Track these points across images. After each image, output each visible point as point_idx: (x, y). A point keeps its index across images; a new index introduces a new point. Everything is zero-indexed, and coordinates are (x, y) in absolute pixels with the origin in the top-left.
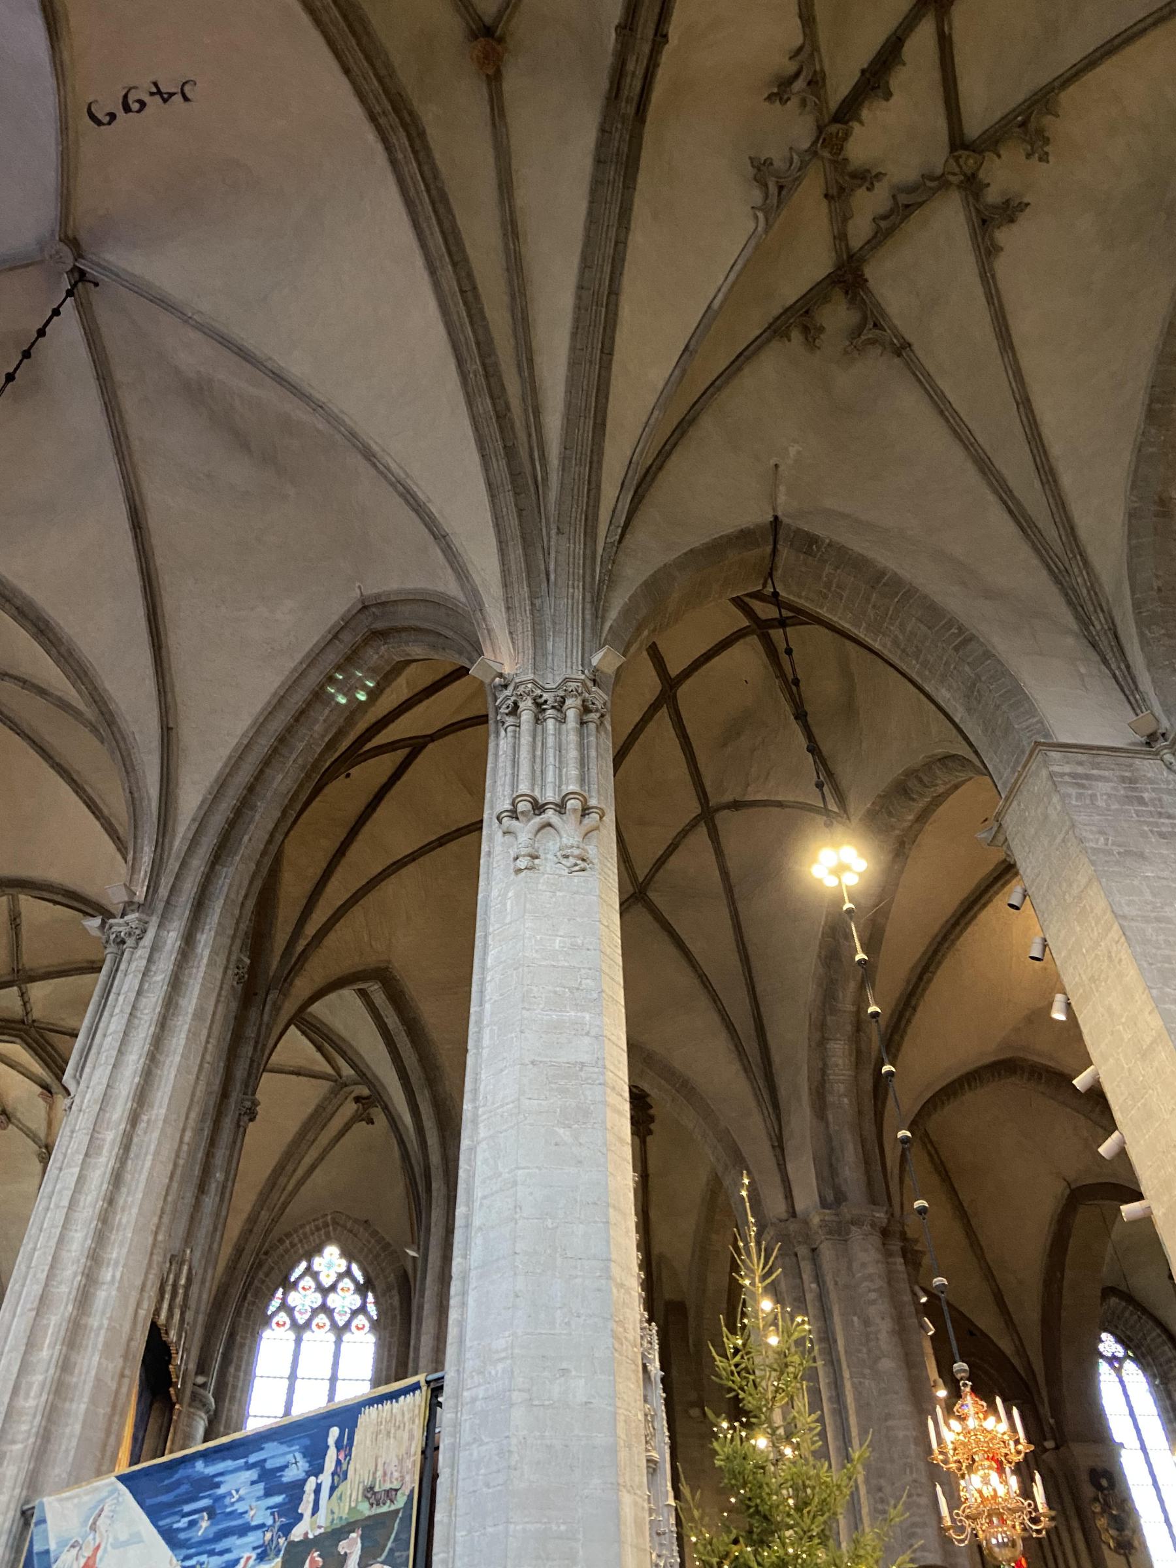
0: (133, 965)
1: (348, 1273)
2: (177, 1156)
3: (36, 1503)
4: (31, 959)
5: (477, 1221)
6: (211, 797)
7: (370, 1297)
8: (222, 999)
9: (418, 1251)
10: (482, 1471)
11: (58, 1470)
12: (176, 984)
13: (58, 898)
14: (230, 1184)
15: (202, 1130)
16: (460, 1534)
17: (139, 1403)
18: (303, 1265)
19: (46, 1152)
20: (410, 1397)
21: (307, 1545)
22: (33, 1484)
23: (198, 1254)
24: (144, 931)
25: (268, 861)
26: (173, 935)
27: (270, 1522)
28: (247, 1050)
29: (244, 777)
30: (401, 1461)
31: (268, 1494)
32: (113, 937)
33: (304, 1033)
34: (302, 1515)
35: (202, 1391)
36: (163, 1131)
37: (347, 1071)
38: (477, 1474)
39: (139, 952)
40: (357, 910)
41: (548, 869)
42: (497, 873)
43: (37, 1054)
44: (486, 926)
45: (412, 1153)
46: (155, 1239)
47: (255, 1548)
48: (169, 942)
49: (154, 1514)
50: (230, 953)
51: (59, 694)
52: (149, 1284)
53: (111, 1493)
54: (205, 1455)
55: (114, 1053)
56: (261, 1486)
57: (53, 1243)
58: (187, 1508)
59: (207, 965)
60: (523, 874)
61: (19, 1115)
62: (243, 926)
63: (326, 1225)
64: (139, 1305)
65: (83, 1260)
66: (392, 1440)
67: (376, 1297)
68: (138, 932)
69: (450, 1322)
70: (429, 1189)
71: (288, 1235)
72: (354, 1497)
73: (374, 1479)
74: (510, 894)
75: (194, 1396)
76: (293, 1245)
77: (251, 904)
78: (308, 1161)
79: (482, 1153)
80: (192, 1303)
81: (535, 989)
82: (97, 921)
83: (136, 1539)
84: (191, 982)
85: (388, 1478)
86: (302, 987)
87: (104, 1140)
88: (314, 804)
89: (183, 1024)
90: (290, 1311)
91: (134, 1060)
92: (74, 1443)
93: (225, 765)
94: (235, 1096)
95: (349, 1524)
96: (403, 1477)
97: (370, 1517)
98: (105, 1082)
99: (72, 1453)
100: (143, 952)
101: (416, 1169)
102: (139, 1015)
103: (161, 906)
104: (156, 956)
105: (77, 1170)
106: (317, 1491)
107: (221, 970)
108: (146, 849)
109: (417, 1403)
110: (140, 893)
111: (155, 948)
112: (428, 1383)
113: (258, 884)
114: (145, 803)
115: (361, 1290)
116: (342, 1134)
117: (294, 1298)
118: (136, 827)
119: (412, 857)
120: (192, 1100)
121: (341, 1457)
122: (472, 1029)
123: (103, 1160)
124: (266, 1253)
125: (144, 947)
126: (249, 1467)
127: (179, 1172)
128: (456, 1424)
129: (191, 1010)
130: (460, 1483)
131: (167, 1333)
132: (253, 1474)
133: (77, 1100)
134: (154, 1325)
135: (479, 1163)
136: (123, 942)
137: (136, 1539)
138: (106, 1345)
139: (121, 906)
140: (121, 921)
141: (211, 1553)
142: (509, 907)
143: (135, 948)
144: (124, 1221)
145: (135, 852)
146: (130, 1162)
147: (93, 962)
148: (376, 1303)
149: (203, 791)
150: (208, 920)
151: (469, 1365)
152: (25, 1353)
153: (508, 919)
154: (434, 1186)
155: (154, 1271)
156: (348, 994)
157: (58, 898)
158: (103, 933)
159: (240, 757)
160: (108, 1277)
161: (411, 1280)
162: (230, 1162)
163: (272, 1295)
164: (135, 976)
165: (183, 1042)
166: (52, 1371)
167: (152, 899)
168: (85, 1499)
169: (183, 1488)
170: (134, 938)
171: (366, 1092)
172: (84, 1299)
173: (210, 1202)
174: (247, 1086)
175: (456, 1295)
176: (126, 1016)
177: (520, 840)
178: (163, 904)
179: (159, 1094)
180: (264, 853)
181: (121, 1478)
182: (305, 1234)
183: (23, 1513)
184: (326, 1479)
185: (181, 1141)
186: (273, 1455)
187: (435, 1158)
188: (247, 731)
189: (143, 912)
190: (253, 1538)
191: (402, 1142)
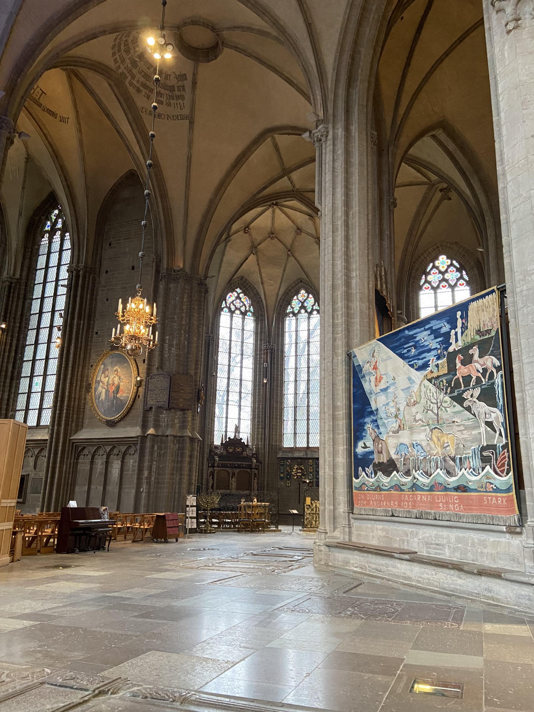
0: (328, 149)
1: (452, 265)
2: (368, 226)
3: (351, 351)
4: (289, 163)
5: (512, 219)
6: (338, 54)
7: (464, 273)
8: (369, 154)
9: (483, 248)
10: (530, 317)
11: (356, 340)
12: (348, 153)
13: (290, 131)
14: (392, 235)
15: (375, 215)
16: (523, 341)
17: (378, 318)
18: (431, 265)
19: (318, 240)
20: (490, 296)
21: (455, 353)
22: (349, 346)
23: (387, 263)
24: (328, 132)
25: (373, 80)
26: (340, 130)
27: (439, 347)
28: (385, 177)
29: (350, 38)
30: (491, 319)
31: (436, 338)
32: (316, 139)
33: (409, 165)
34: (451, 343)
35: (401, 316)
36: (359, 218)
37: (434, 178)
38: (528, 319)
39: (328, 143)
40: (423, 94)
41: (527, 25)
42: (496, 38)
43: (302, 202)
44: (494, 71)
45: (472, 207)
46: (368, 259)
47: (435, 356)
48: (339, 134)
49: (393, 349)
50: (367, 131)
51: (257, 27)
52: (370, 275)
53: (376, 345)
54: (408, 328)
55: (331, 189)
56: (433, 335)
57: (331, 267)
58: (405, 346)
59: (359, 140)
60: (512, 33)
61: (304, 228)
62: (369, 117)
63: (438, 247)
64: (368, 284)
65: (343, 270)
66: (485, 312)
67: (466, 272)
68: (325, 133)
69: (505, 264)
70: (484, 221)
71: (422, 254)
72: (472, 334)
73: (480, 327)
74: (506, 47)
75: (398, 318)
76: (425, 258)
77: (370, 104)
78: (423, 222)
79: (511, 187)
80: (389, 281)
81: (529, 97)
82: (307, 134)
83: (389, 358)
84: (354, 150)
85: (486, 326)
86: (404, 141)
87: (338, 225)
88: (388, 42)
89: (355, 170)
90: (429, 283)
91: (340, 164)
92: (358, 332)
93: (340, 35)
94: (385, 199)
95: (471, 344)
96: (492, 325)
97: (480, 340)
98: (331, 202)
99: (359, 335)
100: (330, 142)
101: (476, 213)
102: (336, 170)
103: (331, 118)
104: (336, 142)
105: (331, 238)
106: (456, 334)
107: (365, 141)
108: (317, 92)
109: (494, 297)
110: (321, 114)
111: (334, 139)
112: (498, 289)
113: (371, 92)
114: (310, 68)
115: (459, 270)
116: (437, 206)
117: (429, 278)
118: (310, 83)
119: (447, 54)
120: (368, 202)
121: (464, 321)
122: (495, 128)
123: (339, 232)
124: (414, 262)
125: (330, 140)
126: (426, 330)
127: (370, 231)
128: (514, 303)
129: (357, 162)
130: (520, 323)
131: (382, 293)
132: (428, 332)
133: (323, 212)
134: (376, 290)
135: (509, 193)
136: (321, 140)
137: (389, 358)
138: (361, 299)
139: (315, 123)
140: (317, 130)
141: (419, 359)
142: (506, 55)
143: (326, 141)
144: (354, 254)
145: (313, 96)
146: (350, 232)
147: (311, 157)
148: (467, 274)
149: (334, 53)
150: (353, 118)
151: (517, 278)
152: (333, 305)
153: (507, 63)
154: (487, 219)
155: (371, 270)
156: (427, 139)
157: (290, 131)
158: (311, 138)
159: (346, 27)
160: (354, 275)
161: (482, 262)
162: (390, 226)
163: (421, 279)
164: (330, 154)
165: (357, 178)
166: (344, 310)
167: (327, 117)
168: (368, 348)
169: (402, 340)
170: (324, 136)
171: (445, 185)
172: (348, 284)
173: (386, 243)
174: (389, 193)
175: (506, 252)
176: (331, 172)
177: (507, 13)
178: (332, 117)
179: (354, 202)
180: (370, 76)
181: (378, 340)
182: (429, 253)
183: (348, 355)
184: (459, 330)
185: (368, 219)
186: (435, 325)
187: (485, 206)
188: (346, 11)
189: (325, 123)
190: (433, 353)
191: (466, 203)
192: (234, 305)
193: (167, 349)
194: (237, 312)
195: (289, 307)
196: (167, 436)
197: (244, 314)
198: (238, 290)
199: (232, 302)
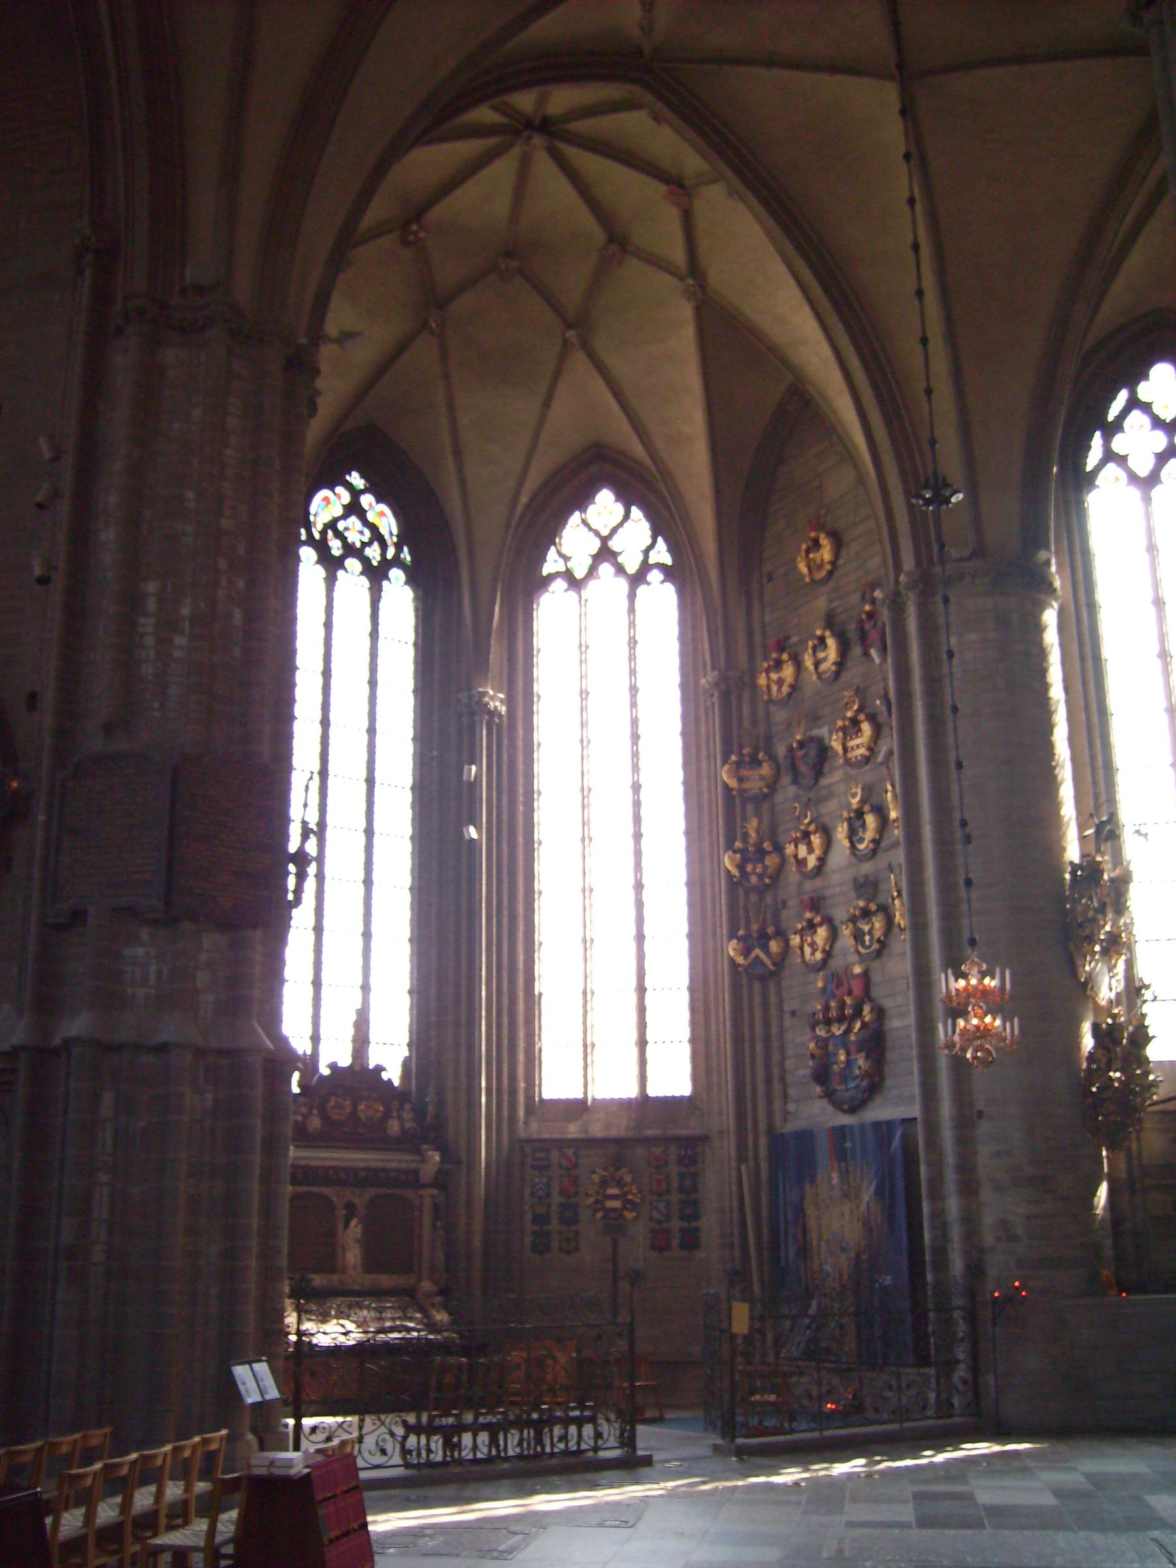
18: (1123, 396)
117: (1119, 444)
192: (339, 535)
193: (149, 641)
194: (353, 564)
195: (552, 553)
196: (163, 1048)
197: (376, 574)
198: (356, 479)
199: (332, 525)
